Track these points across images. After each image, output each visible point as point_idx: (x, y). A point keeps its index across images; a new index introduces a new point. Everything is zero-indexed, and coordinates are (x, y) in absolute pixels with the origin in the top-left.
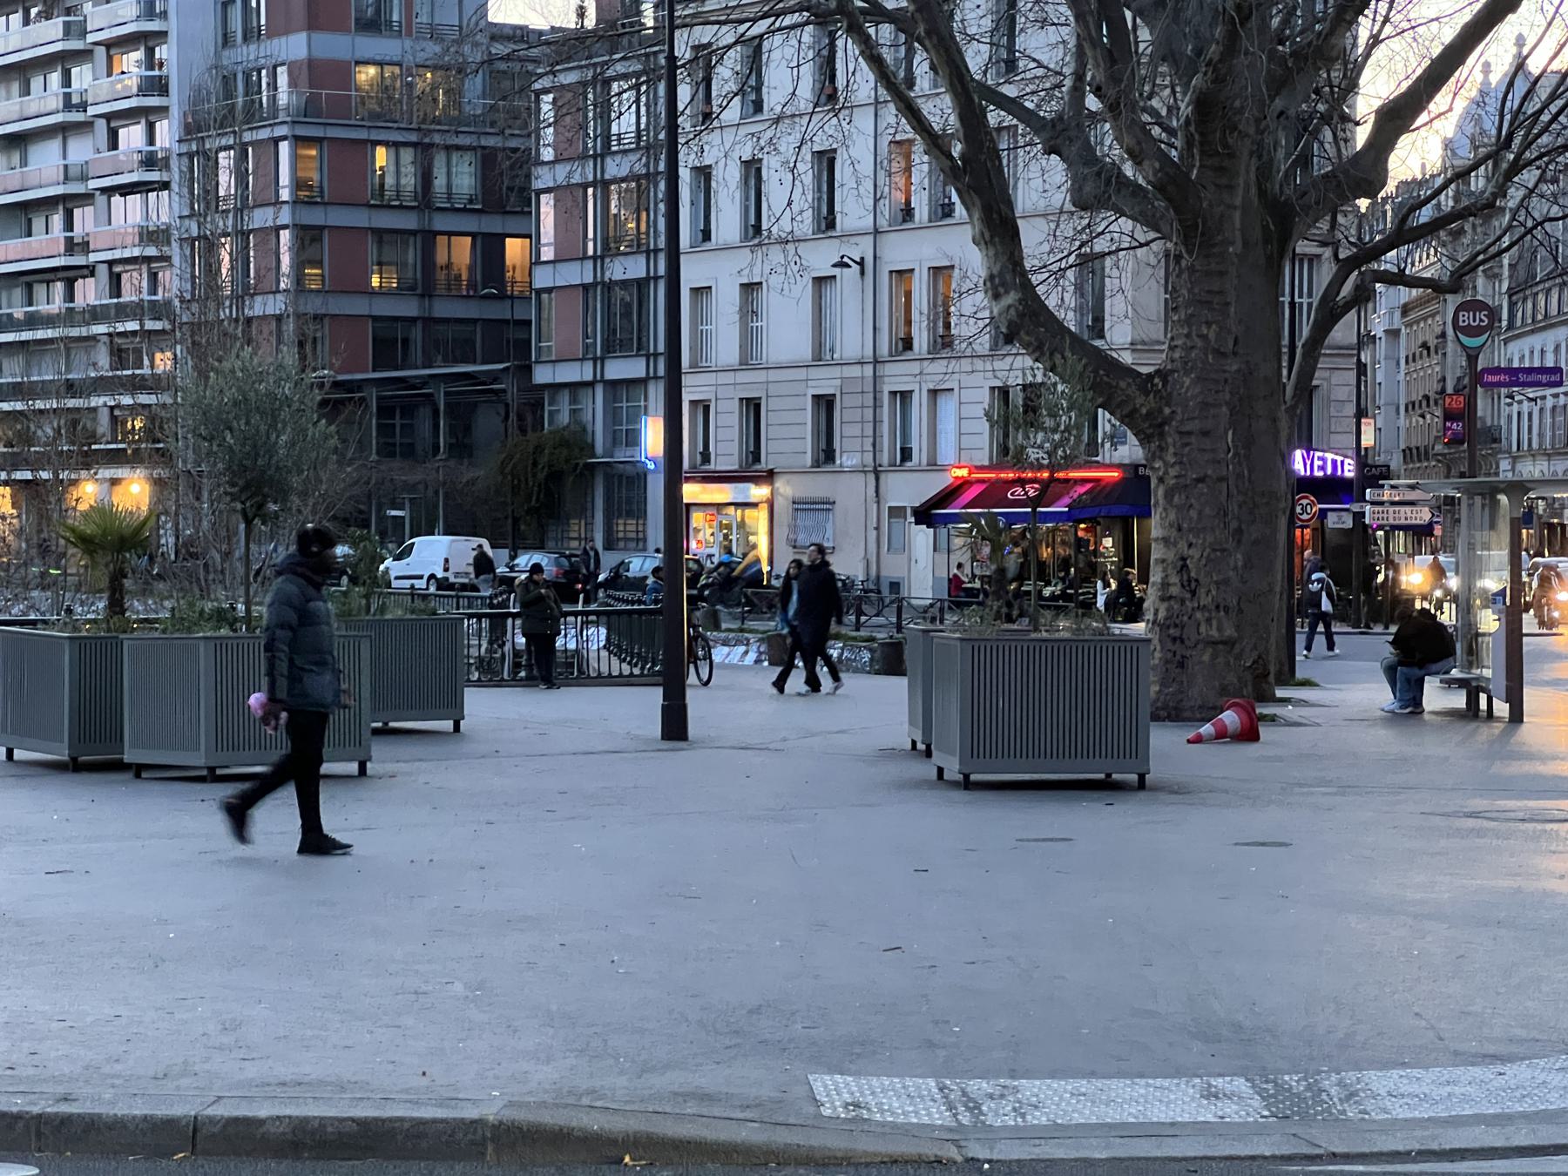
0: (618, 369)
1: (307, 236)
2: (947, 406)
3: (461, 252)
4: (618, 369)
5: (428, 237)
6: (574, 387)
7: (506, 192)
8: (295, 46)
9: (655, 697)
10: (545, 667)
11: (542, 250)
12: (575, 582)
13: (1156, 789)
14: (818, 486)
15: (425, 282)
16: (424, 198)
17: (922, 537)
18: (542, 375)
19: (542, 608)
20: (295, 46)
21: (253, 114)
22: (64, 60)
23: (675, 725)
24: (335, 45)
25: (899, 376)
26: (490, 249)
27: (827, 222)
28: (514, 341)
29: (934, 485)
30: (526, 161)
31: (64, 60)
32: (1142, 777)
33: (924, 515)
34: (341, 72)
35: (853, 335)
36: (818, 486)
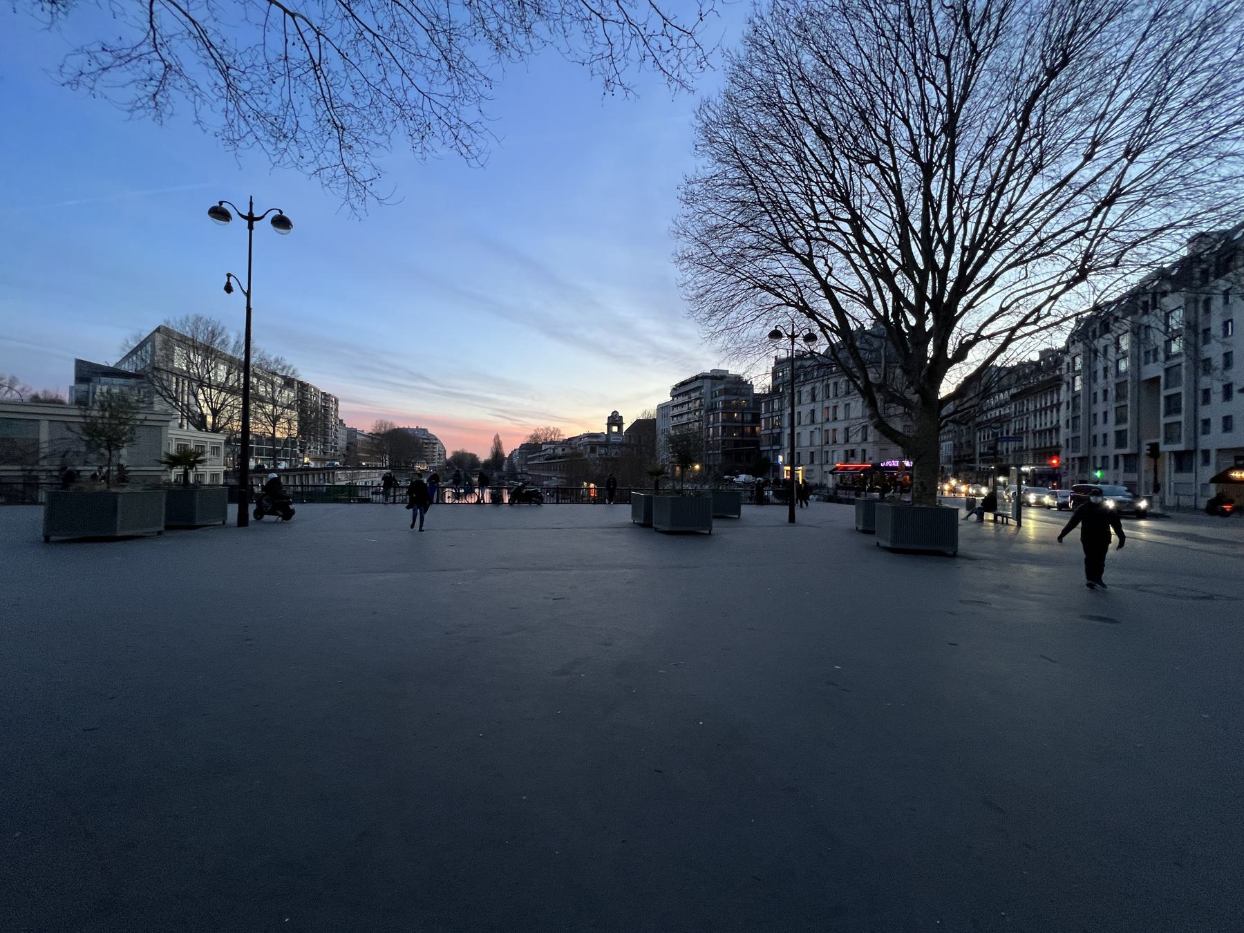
0: (775, 447)
1: (724, 428)
2: (836, 454)
3: (749, 430)
4: (775, 447)
5: (743, 428)
7: (756, 419)
8: (723, 398)
9: (787, 508)
10: (761, 500)
11: (762, 429)
12: (766, 483)
14: (811, 467)
15: (743, 434)
16: (743, 421)
17: (830, 476)
19: (760, 488)
20: (723, 398)
21: (716, 409)
22: (688, 402)
23: (792, 518)
24: (728, 398)
25: (826, 448)
26: (753, 429)
27: (813, 422)
28: (757, 443)
29: (832, 468)
30: (759, 414)
31: (688, 402)
33: (831, 472)
34: (730, 402)
35: (817, 441)
36: (811, 467)
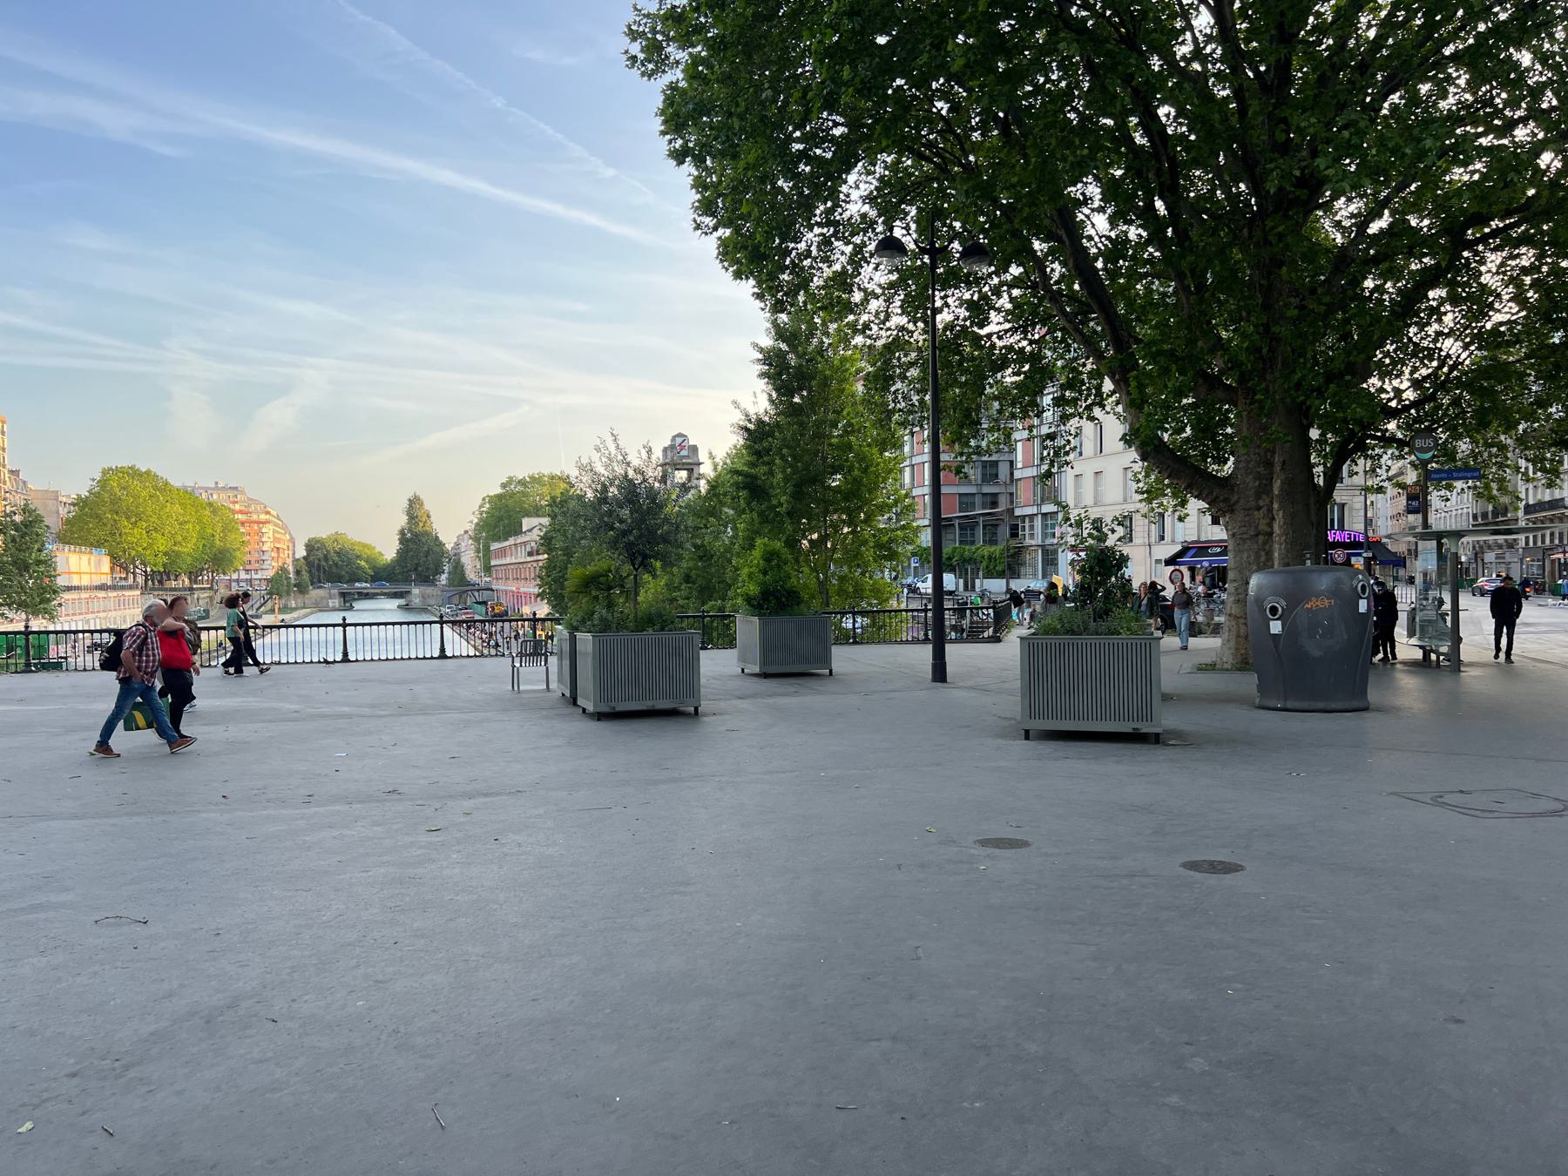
6: (1031, 517)
9: (927, 651)
13: (705, 715)
18: (1018, 512)
23: (939, 672)
32: (696, 709)
